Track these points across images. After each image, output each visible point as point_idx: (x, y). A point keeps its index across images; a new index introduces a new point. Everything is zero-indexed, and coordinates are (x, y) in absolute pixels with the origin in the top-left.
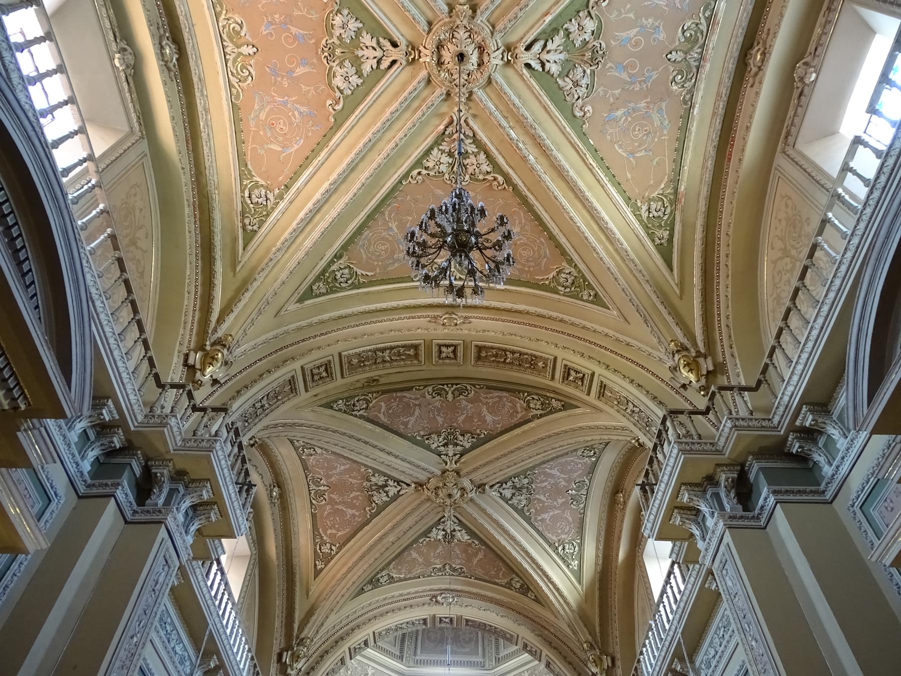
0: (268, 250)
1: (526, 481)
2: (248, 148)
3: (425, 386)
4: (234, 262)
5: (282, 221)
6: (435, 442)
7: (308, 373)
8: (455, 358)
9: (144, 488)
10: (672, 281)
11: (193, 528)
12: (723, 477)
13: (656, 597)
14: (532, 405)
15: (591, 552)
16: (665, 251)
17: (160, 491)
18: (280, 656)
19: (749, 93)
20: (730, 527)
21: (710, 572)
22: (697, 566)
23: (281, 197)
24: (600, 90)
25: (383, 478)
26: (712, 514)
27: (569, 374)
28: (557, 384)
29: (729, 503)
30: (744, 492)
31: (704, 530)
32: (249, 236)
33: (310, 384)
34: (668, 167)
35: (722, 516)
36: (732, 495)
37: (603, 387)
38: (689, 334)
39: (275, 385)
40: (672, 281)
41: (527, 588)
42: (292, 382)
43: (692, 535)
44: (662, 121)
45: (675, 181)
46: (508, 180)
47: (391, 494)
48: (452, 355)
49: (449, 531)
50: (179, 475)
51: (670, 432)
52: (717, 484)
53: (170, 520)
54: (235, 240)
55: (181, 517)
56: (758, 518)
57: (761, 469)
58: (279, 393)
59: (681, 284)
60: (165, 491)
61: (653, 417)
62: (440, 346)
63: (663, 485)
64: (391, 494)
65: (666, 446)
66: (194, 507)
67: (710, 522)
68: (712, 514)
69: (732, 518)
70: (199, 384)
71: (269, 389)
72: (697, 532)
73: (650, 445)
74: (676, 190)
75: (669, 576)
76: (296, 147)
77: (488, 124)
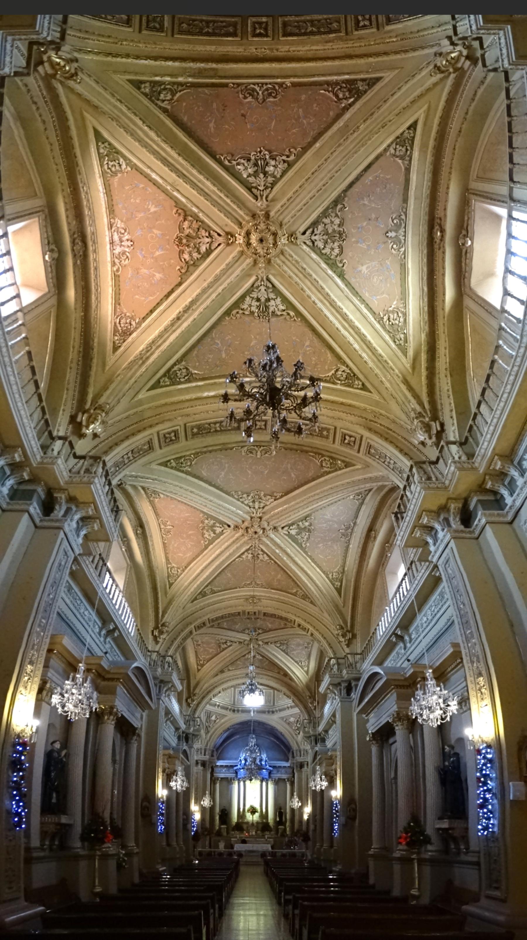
0: (179, 589)
1: (307, 524)
2: (170, 556)
3: (242, 447)
4: (166, 593)
5: (140, 341)
6: (248, 501)
7: (161, 436)
8: (266, 429)
9: (48, 507)
10: (340, 602)
11: (83, 533)
12: (453, 506)
13: (391, 595)
14: (324, 465)
15: (313, 665)
16: (339, 590)
17: (60, 508)
18: (153, 632)
19: (370, 544)
20: (454, 538)
21: (436, 566)
22: (427, 563)
23: (183, 571)
24: (312, 539)
25: (212, 522)
26: (443, 530)
27: (345, 439)
28: (337, 446)
29: (456, 524)
30: (467, 518)
31: (435, 540)
32: (171, 585)
33: (163, 444)
34: (340, 562)
35: (449, 531)
36: (458, 519)
37: (370, 447)
38: (345, 622)
39: (137, 444)
40: (340, 602)
41: (286, 675)
42: (150, 443)
43: (427, 543)
44: (338, 548)
45: (343, 566)
46: (275, 562)
47: (217, 532)
48: (263, 427)
49: (263, 300)
50: (71, 499)
51: (416, 476)
52: (448, 511)
53: (67, 528)
54: (165, 585)
55: (74, 525)
56: (473, 532)
57: (479, 501)
58: (141, 449)
59: (344, 602)
60: (64, 508)
61: (403, 467)
62: (267, 36)
63: (410, 512)
64: (217, 532)
65: (412, 486)
66: (83, 519)
67: (441, 534)
68: (443, 530)
69: (456, 531)
70: (82, 436)
71: (133, 446)
72: (430, 541)
73: (402, 487)
74: (344, 569)
75: (399, 588)
76: (189, 555)
77: (267, 546)
